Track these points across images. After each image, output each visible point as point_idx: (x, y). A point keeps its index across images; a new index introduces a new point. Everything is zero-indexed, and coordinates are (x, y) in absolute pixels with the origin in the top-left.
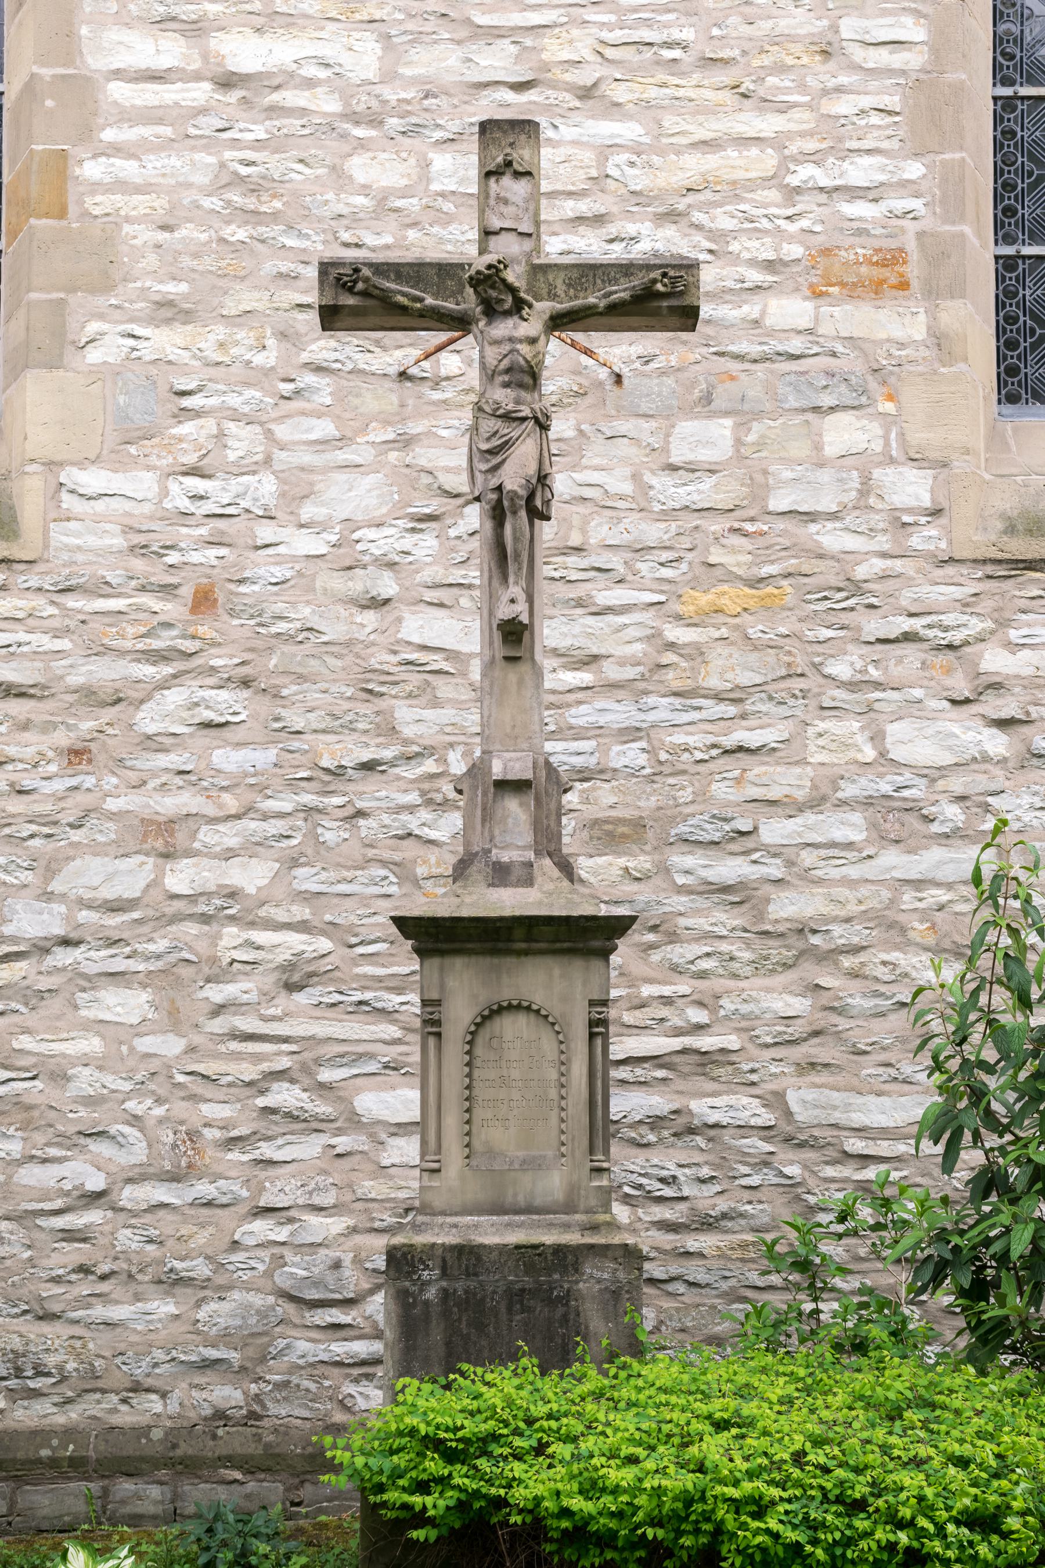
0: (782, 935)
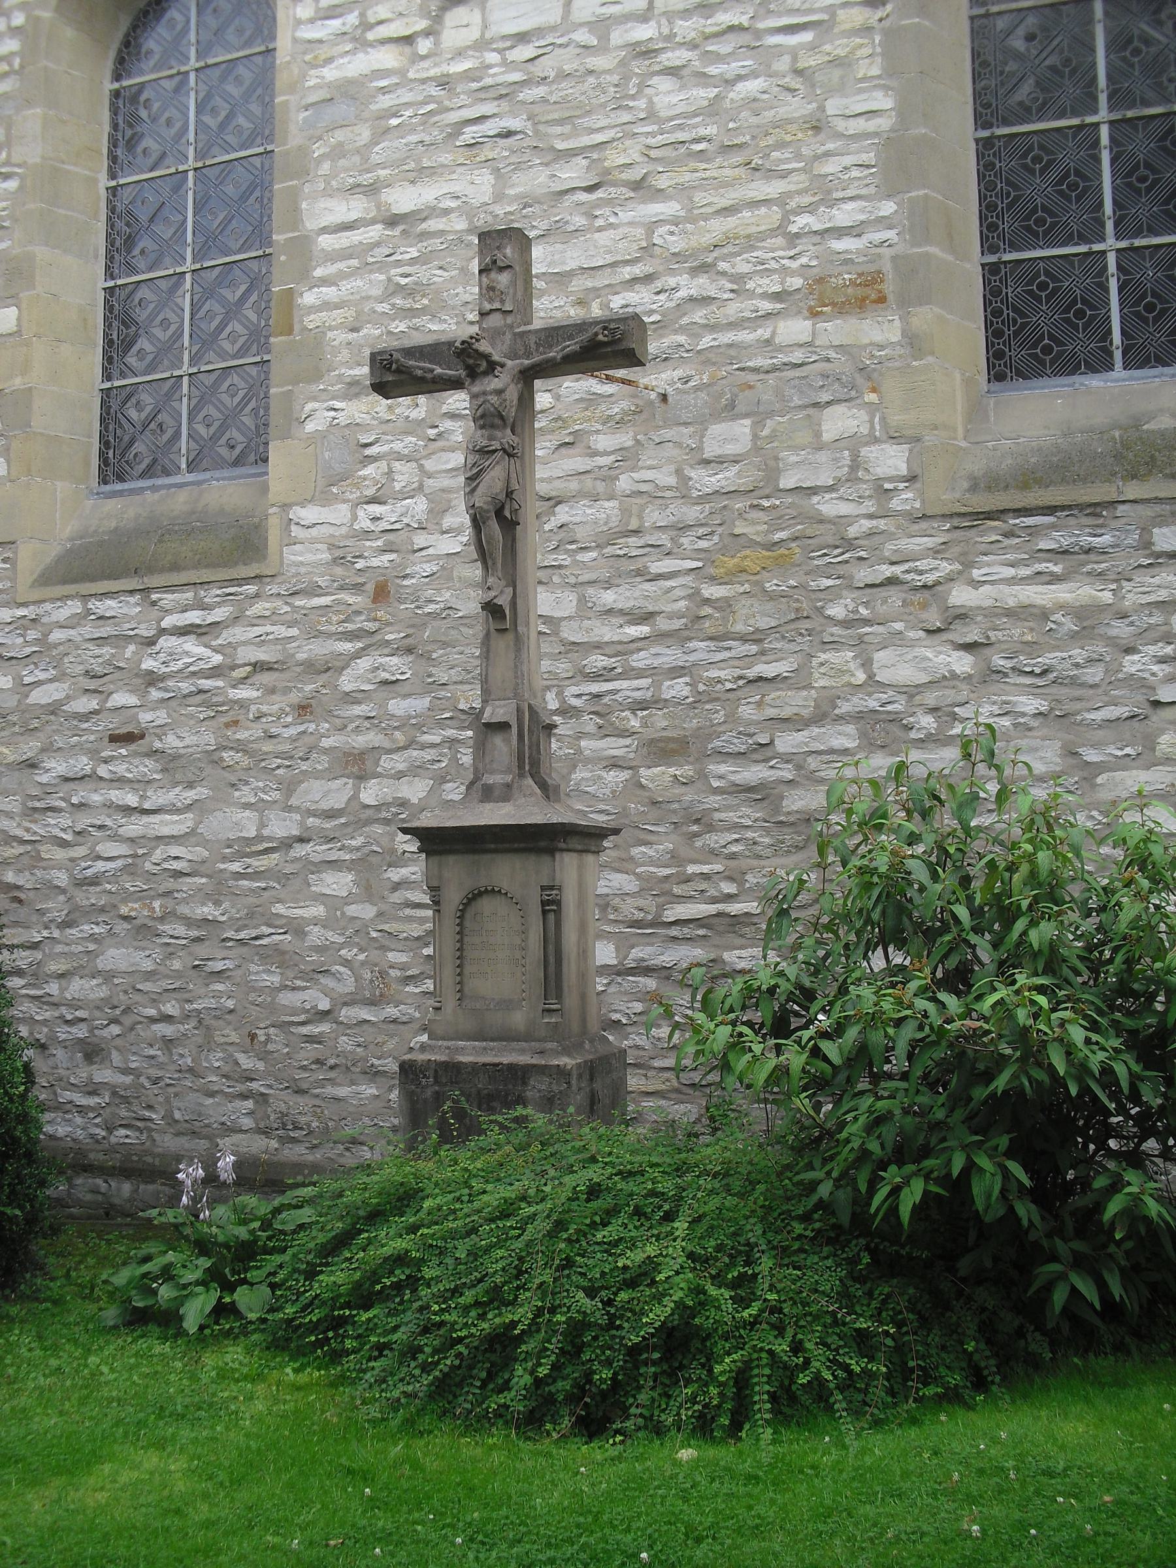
0: (793, 824)
